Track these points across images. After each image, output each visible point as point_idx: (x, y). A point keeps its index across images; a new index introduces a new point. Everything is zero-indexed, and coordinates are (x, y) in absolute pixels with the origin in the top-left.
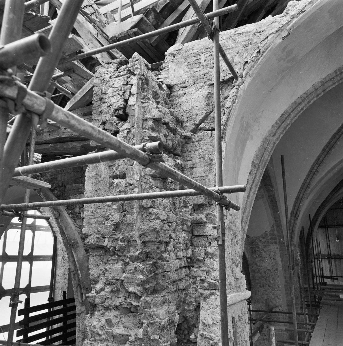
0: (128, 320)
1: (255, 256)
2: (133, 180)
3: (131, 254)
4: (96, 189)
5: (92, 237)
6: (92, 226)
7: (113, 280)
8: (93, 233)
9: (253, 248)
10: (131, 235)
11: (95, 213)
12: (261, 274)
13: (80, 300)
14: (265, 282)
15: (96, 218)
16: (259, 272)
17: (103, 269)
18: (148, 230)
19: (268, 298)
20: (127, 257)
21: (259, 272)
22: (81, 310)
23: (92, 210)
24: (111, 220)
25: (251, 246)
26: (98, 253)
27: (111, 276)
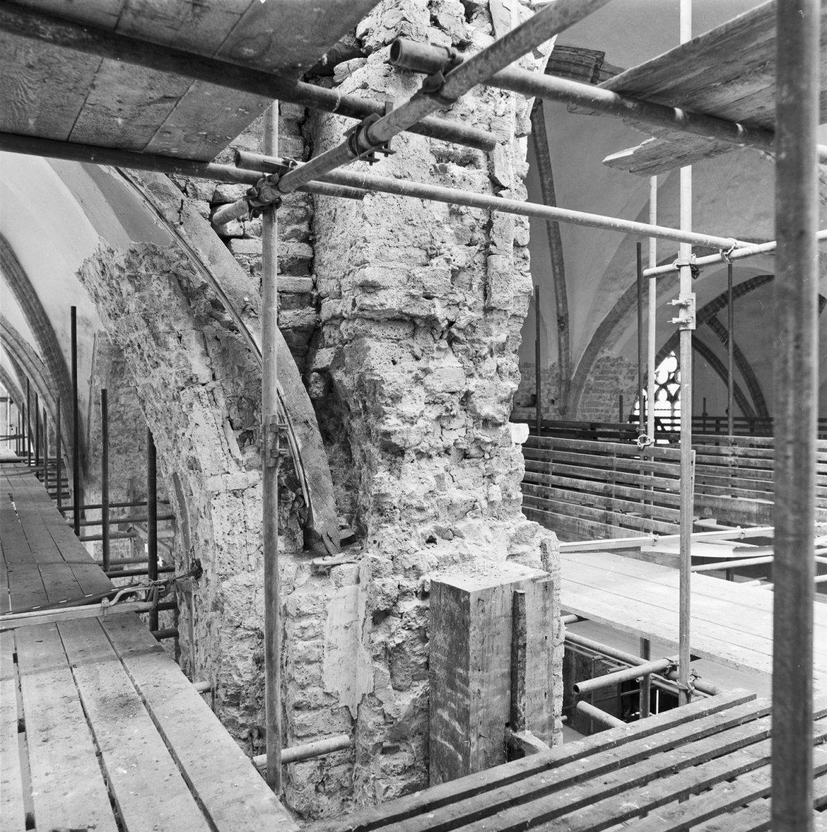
0: (467, 473)
1: (119, 383)
2: (507, 178)
3: (493, 339)
4: (398, 174)
5: (392, 292)
6: (391, 265)
7: (444, 394)
8: (397, 283)
9: (118, 363)
10: (506, 299)
11: (400, 234)
12: (124, 423)
13: (240, 457)
14: (131, 441)
15: (403, 248)
16: (120, 418)
17: (415, 369)
18: (519, 291)
19: (135, 477)
20: (485, 343)
21: (120, 418)
22: (246, 480)
23: (390, 225)
24: (445, 259)
25: (114, 359)
26: (393, 334)
27: (441, 384)
